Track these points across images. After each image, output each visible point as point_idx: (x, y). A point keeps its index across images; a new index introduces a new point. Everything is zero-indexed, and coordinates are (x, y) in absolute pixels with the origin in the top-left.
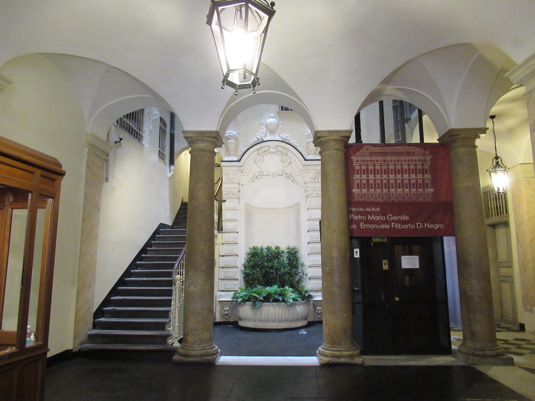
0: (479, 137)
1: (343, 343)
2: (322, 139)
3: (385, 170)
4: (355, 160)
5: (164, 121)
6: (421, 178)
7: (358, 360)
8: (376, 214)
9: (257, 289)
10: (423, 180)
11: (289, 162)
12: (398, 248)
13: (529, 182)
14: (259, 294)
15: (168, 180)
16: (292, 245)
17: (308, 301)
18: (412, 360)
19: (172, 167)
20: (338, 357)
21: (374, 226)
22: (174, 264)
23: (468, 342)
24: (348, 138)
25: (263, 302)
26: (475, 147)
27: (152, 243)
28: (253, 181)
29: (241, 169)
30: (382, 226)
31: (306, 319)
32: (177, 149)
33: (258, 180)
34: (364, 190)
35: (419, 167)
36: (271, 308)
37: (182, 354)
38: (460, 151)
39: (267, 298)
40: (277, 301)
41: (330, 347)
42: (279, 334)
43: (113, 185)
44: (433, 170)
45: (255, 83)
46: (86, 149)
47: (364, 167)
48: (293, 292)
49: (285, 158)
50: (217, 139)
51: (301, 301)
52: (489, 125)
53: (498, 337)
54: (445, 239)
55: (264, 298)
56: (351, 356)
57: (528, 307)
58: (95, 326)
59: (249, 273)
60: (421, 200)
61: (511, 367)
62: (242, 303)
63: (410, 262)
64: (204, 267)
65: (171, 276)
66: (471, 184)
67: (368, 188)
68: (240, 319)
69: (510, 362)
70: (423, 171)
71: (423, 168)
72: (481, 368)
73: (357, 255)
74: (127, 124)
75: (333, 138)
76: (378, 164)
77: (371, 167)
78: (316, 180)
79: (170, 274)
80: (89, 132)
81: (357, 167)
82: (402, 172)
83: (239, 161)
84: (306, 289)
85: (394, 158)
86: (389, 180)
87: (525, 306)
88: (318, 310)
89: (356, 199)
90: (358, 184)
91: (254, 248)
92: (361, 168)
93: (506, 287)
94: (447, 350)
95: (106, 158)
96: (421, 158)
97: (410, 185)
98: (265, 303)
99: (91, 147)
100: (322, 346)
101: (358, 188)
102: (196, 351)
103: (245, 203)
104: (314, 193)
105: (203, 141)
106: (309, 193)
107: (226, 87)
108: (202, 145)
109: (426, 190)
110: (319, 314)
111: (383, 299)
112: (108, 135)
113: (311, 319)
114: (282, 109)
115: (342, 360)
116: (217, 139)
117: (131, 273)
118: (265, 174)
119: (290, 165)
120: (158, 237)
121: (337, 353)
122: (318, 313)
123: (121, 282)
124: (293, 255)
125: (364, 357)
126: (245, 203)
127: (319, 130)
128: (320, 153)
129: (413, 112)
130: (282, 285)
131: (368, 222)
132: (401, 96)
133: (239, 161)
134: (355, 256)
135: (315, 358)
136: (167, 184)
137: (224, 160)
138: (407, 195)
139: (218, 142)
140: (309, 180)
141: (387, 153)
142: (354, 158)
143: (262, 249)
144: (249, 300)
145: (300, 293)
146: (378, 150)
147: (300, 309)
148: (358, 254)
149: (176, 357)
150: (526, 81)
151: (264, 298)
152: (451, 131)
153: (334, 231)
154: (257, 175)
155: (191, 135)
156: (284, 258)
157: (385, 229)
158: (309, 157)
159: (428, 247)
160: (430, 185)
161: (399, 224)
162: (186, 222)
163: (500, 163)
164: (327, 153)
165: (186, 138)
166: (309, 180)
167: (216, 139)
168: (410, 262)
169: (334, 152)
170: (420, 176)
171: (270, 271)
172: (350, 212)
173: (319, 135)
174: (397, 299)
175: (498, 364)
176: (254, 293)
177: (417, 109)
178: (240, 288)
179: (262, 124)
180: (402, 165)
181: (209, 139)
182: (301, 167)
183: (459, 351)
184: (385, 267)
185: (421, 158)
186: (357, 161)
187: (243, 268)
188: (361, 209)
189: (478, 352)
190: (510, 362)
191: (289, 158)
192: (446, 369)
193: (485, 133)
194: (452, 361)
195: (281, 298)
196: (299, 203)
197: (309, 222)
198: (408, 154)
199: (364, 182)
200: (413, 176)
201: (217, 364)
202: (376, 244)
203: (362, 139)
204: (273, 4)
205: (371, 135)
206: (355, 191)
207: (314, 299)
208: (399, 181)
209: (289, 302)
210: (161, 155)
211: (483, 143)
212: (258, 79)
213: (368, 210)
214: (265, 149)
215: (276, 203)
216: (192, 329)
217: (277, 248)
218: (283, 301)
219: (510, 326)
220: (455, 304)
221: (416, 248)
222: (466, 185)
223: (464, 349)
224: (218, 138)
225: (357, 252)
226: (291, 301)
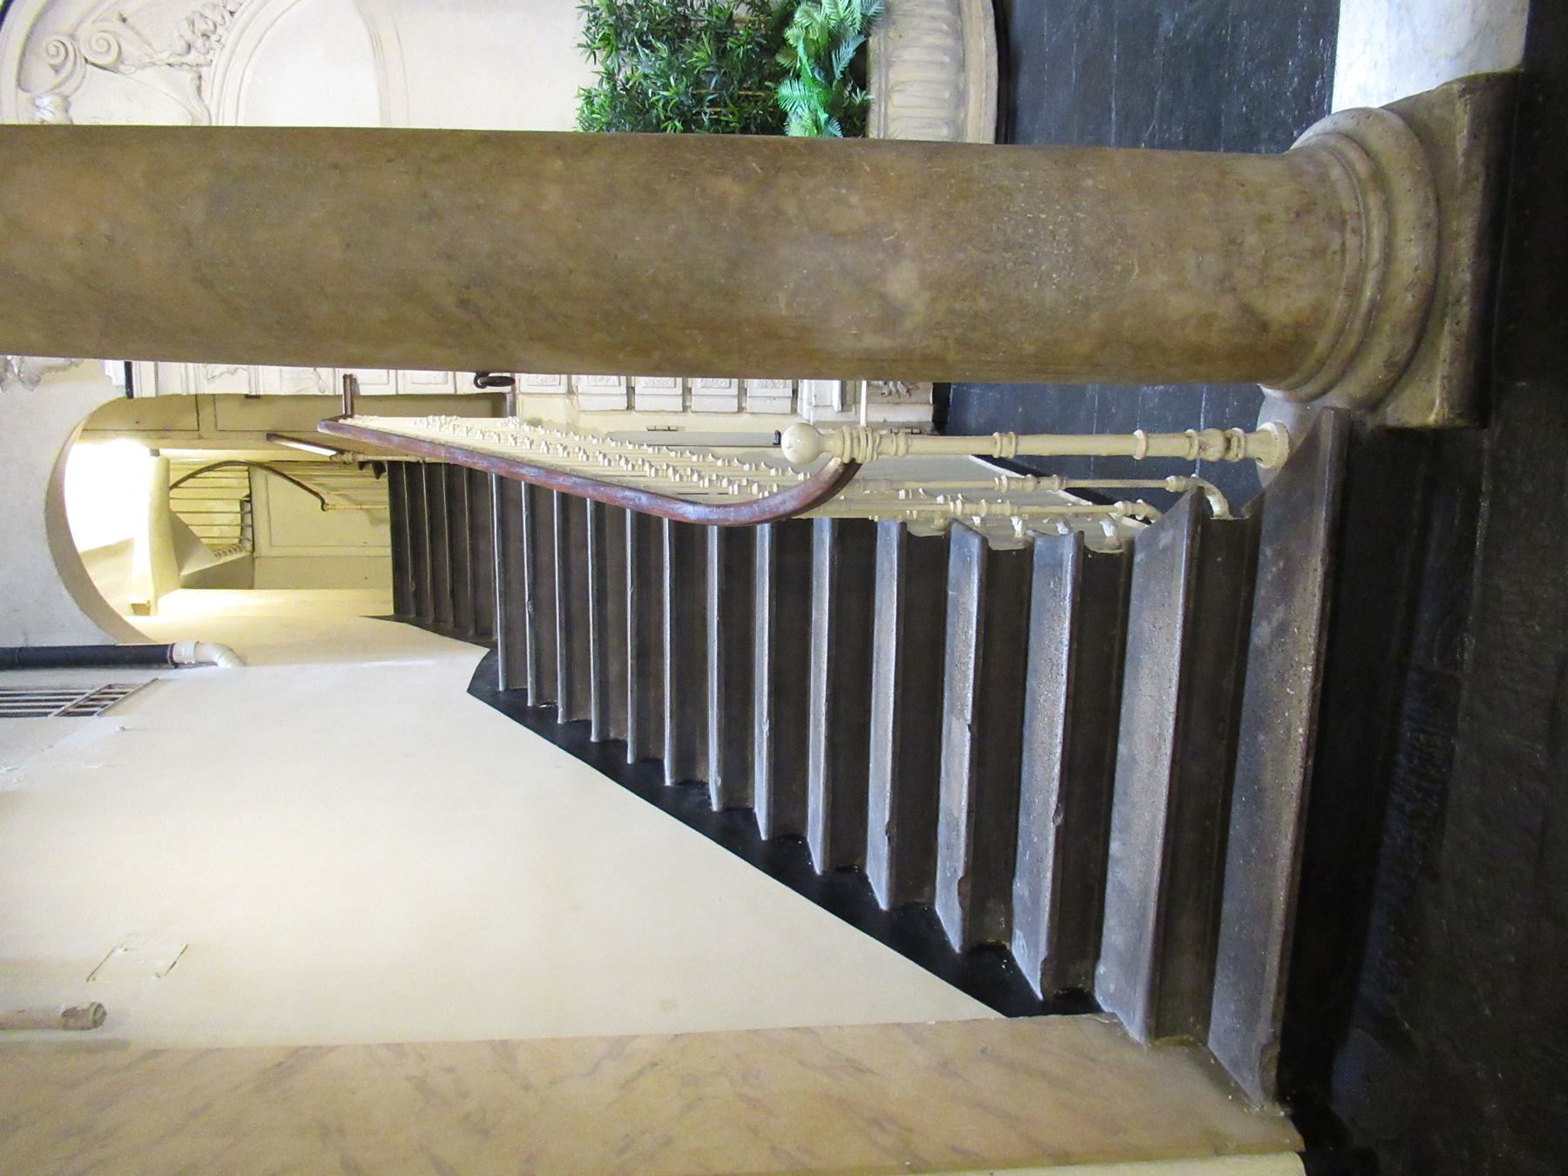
15: (252, 670)
19: (182, 652)
27: (569, 724)
32: (84, 634)
40: (858, 73)
43: (162, 965)
58: (1072, 997)
64: (727, 185)
117: (727, 809)
120: (539, 697)
123: (781, 859)
136: (263, 674)
156: (638, 67)
195: (847, 53)
210: (88, 707)
216: (1225, 283)
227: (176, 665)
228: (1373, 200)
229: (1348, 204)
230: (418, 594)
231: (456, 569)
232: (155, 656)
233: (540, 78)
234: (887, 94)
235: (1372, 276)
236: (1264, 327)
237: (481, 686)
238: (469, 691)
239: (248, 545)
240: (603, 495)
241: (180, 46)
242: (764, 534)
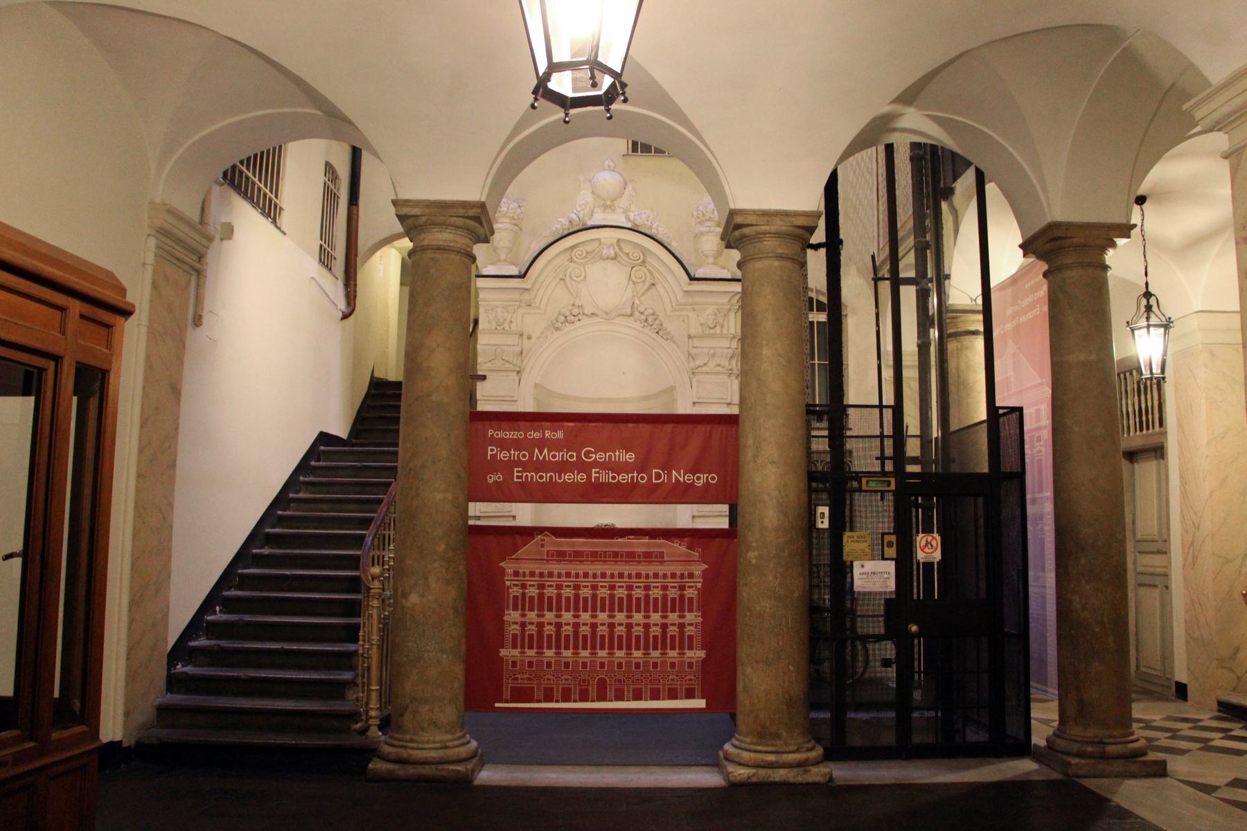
0: (1114, 245)
2: (746, 231)
13: (1213, 355)
20: (771, 766)
21: (546, 477)
22: (363, 537)
24: (811, 230)
26: (1105, 268)
28: (557, 329)
29: (526, 297)
33: (569, 327)
37: (392, 757)
41: (752, 743)
46: (152, 242)
49: (641, 272)
50: (481, 224)
52: (1135, 219)
53: (1135, 715)
54: (986, 470)
65: (357, 568)
66: (1093, 357)
69: (1160, 770)
72: (1091, 784)
75: (773, 228)
78: (718, 329)
79: (354, 562)
80: (158, 200)
83: (523, 276)
93: (1150, 598)
94: (1023, 748)
95: (197, 265)
99: (164, 239)
100: (734, 741)
103: (536, 385)
104: (712, 364)
105: (444, 225)
106: (698, 363)
107: (542, 103)
108: (442, 237)
112: (203, 209)
114: (635, 150)
115: (779, 775)
116: (481, 224)
118: (587, 311)
119: (653, 289)
126: (536, 385)
128: (740, 265)
132: (936, 134)
133: (523, 276)
137: (485, 272)
139: (480, 230)
148: (826, 521)
149: (376, 765)
150: (1233, 121)
152: (1053, 226)
154: (567, 313)
155: (415, 211)
158: (700, 273)
162: (398, 431)
164: (758, 265)
165: (402, 218)
166: (700, 331)
167: (476, 221)
169: (776, 263)
177: (972, 169)
181: (460, 221)
182: (680, 295)
190: (1160, 770)
191: (650, 272)
192: (1018, 787)
194: (1029, 773)
196: (673, 388)
201: (476, 783)
210: (325, 259)
211: (1121, 260)
212: (624, 85)
214: (589, 248)
220: (1044, 635)
224: (483, 220)
228: (438, 745)
233: (14, 412)
235: (415, 745)
236: (402, 715)
237: (324, 438)
238: (1020, 410)
241: (641, 309)
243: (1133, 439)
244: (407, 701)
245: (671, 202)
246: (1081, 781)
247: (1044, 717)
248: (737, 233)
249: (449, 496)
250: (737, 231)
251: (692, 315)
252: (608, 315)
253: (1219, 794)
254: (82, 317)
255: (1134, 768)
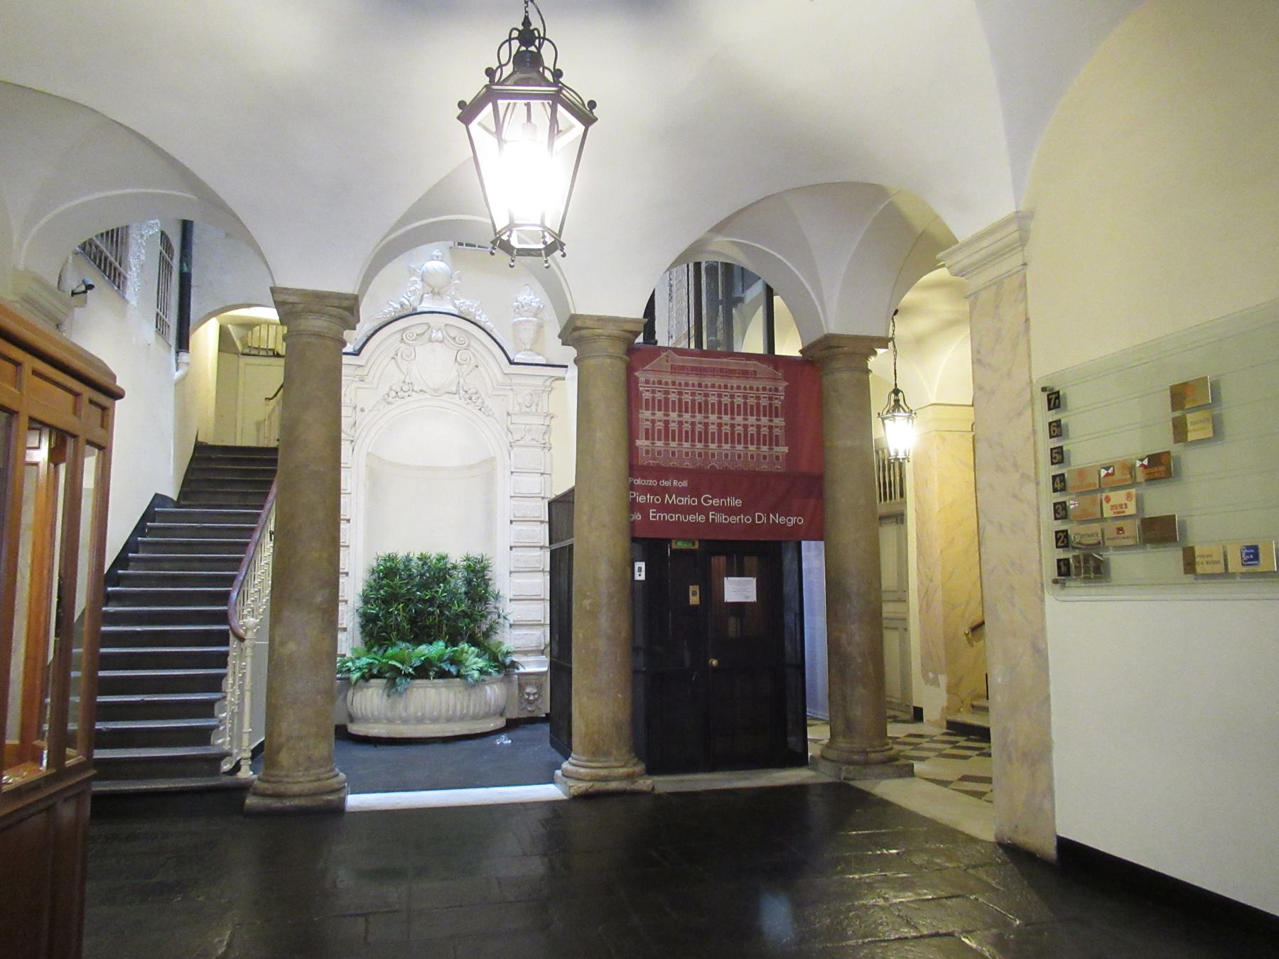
1: (615, 752)
2: (584, 332)
3: (700, 404)
4: (642, 379)
5: (167, 238)
6: (768, 424)
7: (645, 783)
8: (680, 492)
9: (396, 650)
10: (771, 428)
11: (473, 363)
12: (719, 562)
14: (402, 663)
16: (475, 553)
17: (508, 675)
18: (740, 780)
19: (184, 357)
20: (605, 779)
21: (675, 517)
23: (840, 739)
25: (413, 677)
26: (868, 371)
28: (389, 403)
30: (691, 518)
31: (502, 714)
33: (400, 402)
34: (659, 444)
35: (764, 402)
36: (432, 692)
37: (270, 792)
38: (840, 377)
39: (423, 671)
40: (443, 674)
42: (451, 748)
44: (790, 409)
45: (550, 249)
47: (659, 396)
48: (478, 656)
49: (464, 355)
51: (495, 674)
55: (415, 669)
56: (630, 777)
57: (931, 675)
59: (377, 615)
60: (764, 467)
61: (909, 780)
62: (361, 682)
63: (739, 589)
67: (667, 438)
68: (352, 719)
70: (771, 412)
71: (771, 405)
73: (640, 576)
74: (97, 247)
75: (607, 332)
76: (688, 390)
77: (673, 397)
78: (533, 408)
80: (21, 267)
81: (646, 395)
82: (732, 410)
84: (504, 648)
85: (718, 381)
86: (706, 425)
87: (925, 676)
88: (529, 694)
89: (643, 460)
90: (647, 430)
91: (391, 558)
92: (654, 398)
94: (799, 759)
96: (769, 385)
97: (745, 438)
98: (418, 681)
101: (647, 439)
102: (297, 784)
103: (368, 454)
105: (320, 313)
106: (517, 437)
109: (776, 449)
110: (530, 702)
111: (687, 663)
113: (514, 713)
115: (613, 785)
120: (150, 528)
121: (603, 772)
122: (528, 700)
124: (477, 573)
125: (657, 778)
126: (368, 454)
127: (579, 312)
129: (750, 286)
130: (453, 642)
131: (663, 508)
134: (637, 578)
135: (551, 786)
136: (169, 398)
138: (739, 456)
140: (517, 408)
141: (705, 370)
142: (640, 376)
143: (408, 559)
144: (379, 675)
145: (494, 658)
146: (689, 361)
147: (494, 692)
148: (643, 574)
149: (251, 801)
151: (415, 669)
152: (828, 338)
153: (604, 526)
155: (292, 299)
156: (458, 582)
157: (697, 524)
159: (771, 559)
160: (782, 441)
161: (723, 514)
163: (901, 403)
164: (593, 362)
168: (739, 589)
169: (608, 361)
170: (764, 420)
171: (428, 611)
172: (632, 487)
173: (579, 323)
174: (714, 662)
175: (889, 777)
176: (392, 658)
178: (354, 650)
179: (412, 272)
180: (732, 397)
183: (822, 757)
184: (694, 600)
185: (769, 385)
186: (647, 382)
187: (359, 604)
188: (652, 482)
189: (855, 757)
190: (908, 772)
192: (799, 791)
193: (886, 347)
195: (453, 670)
196: (493, 459)
197: (514, 502)
198: (745, 374)
199: (660, 425)
200: (752, 420)
202: (678, 553)
203: (657, 337)
204: (592, 104)
205: (671, 330)
206: (641, 443)
207: (522, 670)
208: (727, 429)
209: (472, 676)
211: (879, 362)
213: (665, 483)
215: (462, 461)
217: (442, 558)
218: (459, 675)
219: (897, 713)
221: (751, 562)
222: (849, 443)
223: (832, 754)
225: (640, 569)
226: (476, 674)
227: (177, 353)
229: (312, 772)
230: (210, 459)
231: (222, 483)
232: (183, 343)
234: (434, 686)
236: (278, 753)
237: (159, 499)
238: (156, 495)
239: (247, 351)
240: (245, 563)
242: (227, 627)
243: (883, 508)
244: (283, 739)
245: (519, 304)
246: (852, 783)
247: (818, 734)
248: (576, 334)
249: (325, 555)
250: (575, 332)
251: (510, 394)
252: (437, 392)
253: (952, 786)
254: (91, 401)
255: (888, 770)
